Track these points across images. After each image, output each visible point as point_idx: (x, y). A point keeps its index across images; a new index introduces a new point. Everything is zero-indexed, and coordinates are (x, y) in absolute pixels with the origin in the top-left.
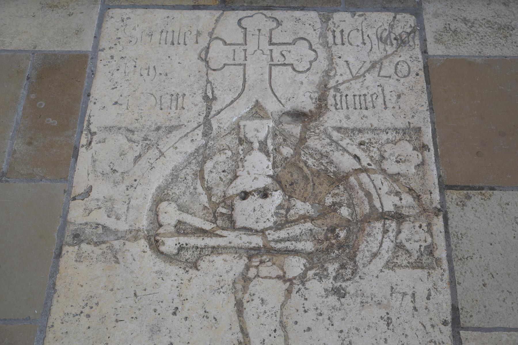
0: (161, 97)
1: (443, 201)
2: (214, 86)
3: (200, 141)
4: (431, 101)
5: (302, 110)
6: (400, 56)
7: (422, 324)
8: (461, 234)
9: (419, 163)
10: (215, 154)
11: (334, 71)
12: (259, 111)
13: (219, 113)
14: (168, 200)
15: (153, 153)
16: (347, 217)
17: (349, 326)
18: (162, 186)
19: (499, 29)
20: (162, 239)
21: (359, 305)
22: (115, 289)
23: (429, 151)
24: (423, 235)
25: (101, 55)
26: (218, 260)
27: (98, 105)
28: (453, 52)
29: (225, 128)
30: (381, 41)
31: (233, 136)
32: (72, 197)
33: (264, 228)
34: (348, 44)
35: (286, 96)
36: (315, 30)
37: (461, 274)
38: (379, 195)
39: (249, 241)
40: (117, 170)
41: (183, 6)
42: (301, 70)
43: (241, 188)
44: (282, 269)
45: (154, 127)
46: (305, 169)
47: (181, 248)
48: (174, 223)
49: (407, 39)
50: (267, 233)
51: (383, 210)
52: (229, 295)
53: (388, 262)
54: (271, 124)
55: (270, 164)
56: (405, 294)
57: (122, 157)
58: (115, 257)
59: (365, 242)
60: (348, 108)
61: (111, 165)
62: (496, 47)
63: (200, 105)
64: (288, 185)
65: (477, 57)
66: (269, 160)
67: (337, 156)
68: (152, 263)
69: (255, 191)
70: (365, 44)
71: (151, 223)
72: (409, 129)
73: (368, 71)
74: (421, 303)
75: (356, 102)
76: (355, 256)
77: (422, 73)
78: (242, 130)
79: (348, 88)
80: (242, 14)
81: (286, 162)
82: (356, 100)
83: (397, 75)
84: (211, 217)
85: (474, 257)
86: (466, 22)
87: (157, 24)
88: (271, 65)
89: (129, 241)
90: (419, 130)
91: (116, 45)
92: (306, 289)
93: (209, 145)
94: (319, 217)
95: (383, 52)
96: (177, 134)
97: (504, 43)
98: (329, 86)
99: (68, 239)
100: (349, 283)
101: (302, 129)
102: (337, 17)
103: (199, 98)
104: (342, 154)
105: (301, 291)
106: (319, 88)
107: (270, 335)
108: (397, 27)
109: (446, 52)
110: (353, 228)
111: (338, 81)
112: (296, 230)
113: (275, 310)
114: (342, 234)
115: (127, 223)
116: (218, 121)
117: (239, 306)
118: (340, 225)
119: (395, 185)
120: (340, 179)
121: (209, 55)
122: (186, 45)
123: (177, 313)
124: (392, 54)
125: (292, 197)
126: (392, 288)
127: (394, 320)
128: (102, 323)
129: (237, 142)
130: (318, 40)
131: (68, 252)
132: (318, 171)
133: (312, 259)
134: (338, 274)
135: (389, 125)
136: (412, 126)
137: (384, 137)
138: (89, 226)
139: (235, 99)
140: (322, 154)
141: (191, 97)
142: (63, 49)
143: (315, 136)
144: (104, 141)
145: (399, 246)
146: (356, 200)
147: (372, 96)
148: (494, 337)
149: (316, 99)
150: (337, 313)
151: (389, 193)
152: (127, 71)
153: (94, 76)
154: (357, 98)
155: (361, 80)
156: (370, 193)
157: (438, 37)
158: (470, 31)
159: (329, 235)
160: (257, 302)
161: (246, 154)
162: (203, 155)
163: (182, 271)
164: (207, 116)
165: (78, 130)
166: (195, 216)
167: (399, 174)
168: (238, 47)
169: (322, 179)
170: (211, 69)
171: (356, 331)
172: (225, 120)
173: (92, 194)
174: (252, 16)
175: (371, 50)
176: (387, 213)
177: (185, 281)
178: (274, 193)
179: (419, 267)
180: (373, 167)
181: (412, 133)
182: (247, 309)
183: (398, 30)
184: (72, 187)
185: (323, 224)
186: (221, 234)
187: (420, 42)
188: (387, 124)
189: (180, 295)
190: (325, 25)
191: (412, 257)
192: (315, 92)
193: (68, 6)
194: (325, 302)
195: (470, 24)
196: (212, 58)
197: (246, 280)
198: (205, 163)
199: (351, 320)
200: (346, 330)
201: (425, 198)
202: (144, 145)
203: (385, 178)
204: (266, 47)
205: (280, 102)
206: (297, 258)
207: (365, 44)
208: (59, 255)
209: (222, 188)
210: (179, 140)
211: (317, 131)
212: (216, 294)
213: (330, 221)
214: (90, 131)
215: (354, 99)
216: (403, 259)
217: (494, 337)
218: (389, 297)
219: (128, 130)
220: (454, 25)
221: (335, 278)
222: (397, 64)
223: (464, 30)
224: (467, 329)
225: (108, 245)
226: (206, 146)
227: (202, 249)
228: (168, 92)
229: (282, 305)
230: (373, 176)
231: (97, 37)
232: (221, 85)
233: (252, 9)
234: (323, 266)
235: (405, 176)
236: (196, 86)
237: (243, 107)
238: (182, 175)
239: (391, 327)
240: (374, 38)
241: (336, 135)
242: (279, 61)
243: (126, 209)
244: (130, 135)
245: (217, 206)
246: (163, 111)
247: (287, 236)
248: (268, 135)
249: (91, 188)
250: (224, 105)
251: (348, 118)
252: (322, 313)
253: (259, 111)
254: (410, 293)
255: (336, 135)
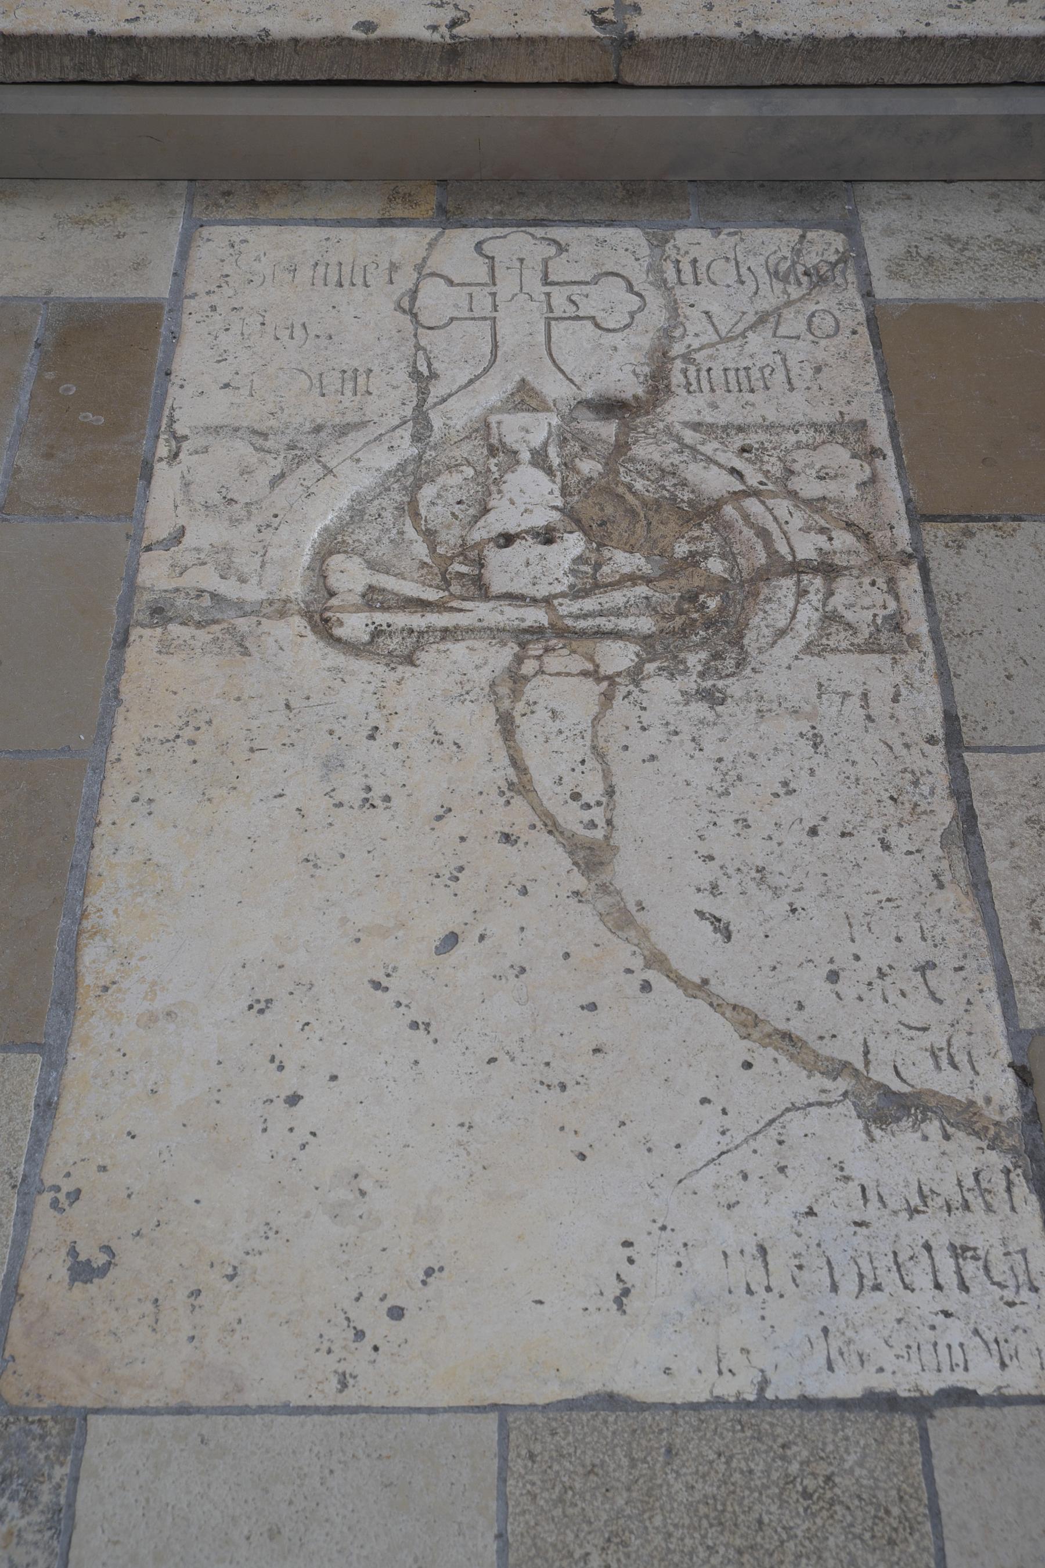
0: (321, 375)
1: (917, 541)
2: (431, 355)
3: (407, 450)
4: (886, 375)
5: (618, 395)
6: (818, 303)
7: (885, 743)
8: (957, 594)
9: (866, 479)
10: (439, 473)
11: (682, 329)
12: (527, 399)
13: (444, 400)
14: (345, 552)
15: (310, 470)
16: (722, 574)
17: (735, 750)
18: (333, 528)
19: (1021, 252)
20: (338, 615)
21: (754, 715)
22: (245, 696)
23: (884, 458)
24: (878, 596)
25: (190, 305)
26: (458, 650)
27: (189, 390)
28: (927, 292)
29: (458, 427)
30: (778, 279)
31: (476, 443)
32: (144, 545)
33: (550, 595)
34: (707, 283)
35: (584, 371)
36: (637, 260)
37: (961, 660)
38: (785, 533)
39: (520, 616)
40: (235, 498)
41: (359, 220)
42: (612, 326)
43: (498, 528)
44: (591, 659)
45: (308, 426)
46: (629, 497)
47: (377, 633)
48: (360, 589)
49: (829, 273)
50: (556, 602)
51: (794, 557)
52: (484, 705)
53: (808, 645)
54: (555, 421)
55: (556, 488)
56: (846, 695)
57: (246, 476)
58: (241, 645)
59: (761, 613)
60: (713, 390)
61: (223, 490)
62: (1015, 283)
63: (404, 387)
64: (594, 526)
65: (976, 300)
66: (554, 482)
67: (694, 472)
68: (318, 655)
69: (527, 532)
70: (743, 283)
71: (313, 591)
72: (841, 424)
73: (752, 327)
74: (879, 707)
75: (730, 380)
76: (742, 637)
77: (864, 330)
78: (494, 430)
79: (711, 357)
80: (482, 233)
81: (588, 486)
82: (729, 378)
83: (813, 334)
84: (438, 580)
85: (986, 631)
86: (952, 243)
87: (305, 251)
88: (548, 321)
89: (269, 618)
90: (862, 426)
91: (220, 287)
92: (642, 691)
93: (427, 457)
94: (662, 577)
95: (781, 295)
96: (359, 438)
97: (1030, 275)
98: (672, 353)
99: (143, 617)
100: (731, 680)
101: (619, 428)
102: (682, 237)
103: (401, 375)
104: (705, 468)
105: (634, 695)
106: (651, 358)
107: (573, 770)
108: (809, 252)
109: (911, 293)
110: (735, 594)
111: (690, 346)
112: (617, 598)
113: (580, 727)
114: (713, 604)
115: (262, 588)
116: (444, 414)
117: (507, 725)
118: (707, 588)
119: (816, 517)
120: (704, 512)
121: (417, 304)
122: (367, 286)
123: (378, 735)
124: (800, 300)
125: (605, 545)
126: (820, 685)
127: (827, 737)
128: (222, 753)
129: (486, 452)
130: (644, 276)
131: (141, 637)
132: (657, 501)
133: (652, 646)
134: (708, 669)
135: (800, 418)
136: (847, 418)
137: (791, 438)
138: (183, 594)
139: (477, 377)
140: (663, 471)
141: (383, 374)
142: (108, 295)
143: (646, 438)
144: (206, 450)
145: (830, 618)
146: (739, 546)
147: (761, 369)
148: (1032, 761)
149: (646, 376)
150: (709, 730)
151: (806, 529)
152: (246, 332)
153: (177, 342)
154: (732, 374)
155: (737, 343)
156: (766, 530)
157: (894, 268)
158: (960, 257)
159: (686, 606)
160: (541, 714)
161: (506, 472)
162: (414, 476)
163: (381, 668)
164: (419, 407)
165: (149, 432)
166: (404, 579)
167: (824, 498)
168: (478, 288)
169: (665, 514)
170: (424, 327)
171: (750, 759)
172: (457, 414)
173: (184, 540)
174: (505, 237)
175: (756, 293)
176: (804, 563)
177: (391, 684)
178: (566, 535)
179: (873, 651)
180: (771, 487)
181: (848, 431)
182: (521, 728)
183: (811, 259)
184: (143, 529)
185: (671, 588)
186: (460, 607)
187: (858, 279)
188: (795, 417)
189: (380, 707)
190: (657, 251)
191: (859, 635)
192: (642, 364)
193: (114, 220)
194: (684, 713)
195: (960, 246)
196: (425, 308)
197: (516, 679)
198: (420, 488)
199: (739, 740)
200: (728, 758)
201: (880, 537)
202: (290, 457)
203: (796, 506)
204: (539, 290)
205: (572, 381)
206: (621, 643)
207: (743, 283)
208: (123, 642)
209: (456, 531)
210: (364, 446)
211: (651, 431)
212: (456, 703)
213: (683, 583)
214: (174, 434)
215: (726, 375)
216: (840, 638)
217: (1032, 761)
218: (814, 700)
219: (255, 432)
220: (927, 247)
221: (702, 675)
222: (813, 315)
223: (948, 255)
224: (977, 749)
225: (225, 625)
226: (421, 458)
227: (421, 633)
228: (336, 366)
229: (595, 719)
230: (770, 502)
231: (179, 276)
232: (447, 353)
233: (503, 226)
234: (677, 657)
235: (838, 502)
236: (393, 356)
237: (493, 391)
238: (373, 509)
239: (821, 749)
240: (761, 272)
241: (689, 436)
242: (565, 312)
243: (259, 564)
244: (259, 441)
245: (449, 562)
246: (326, 398)
247: (599, 607)
248: (548, 438)
249: (183, 530)
250: (455, 388)
251: (714, 406)
252: (678, 730)
253: (527, 399)
254: (859, 692)
255: (689, 436)
